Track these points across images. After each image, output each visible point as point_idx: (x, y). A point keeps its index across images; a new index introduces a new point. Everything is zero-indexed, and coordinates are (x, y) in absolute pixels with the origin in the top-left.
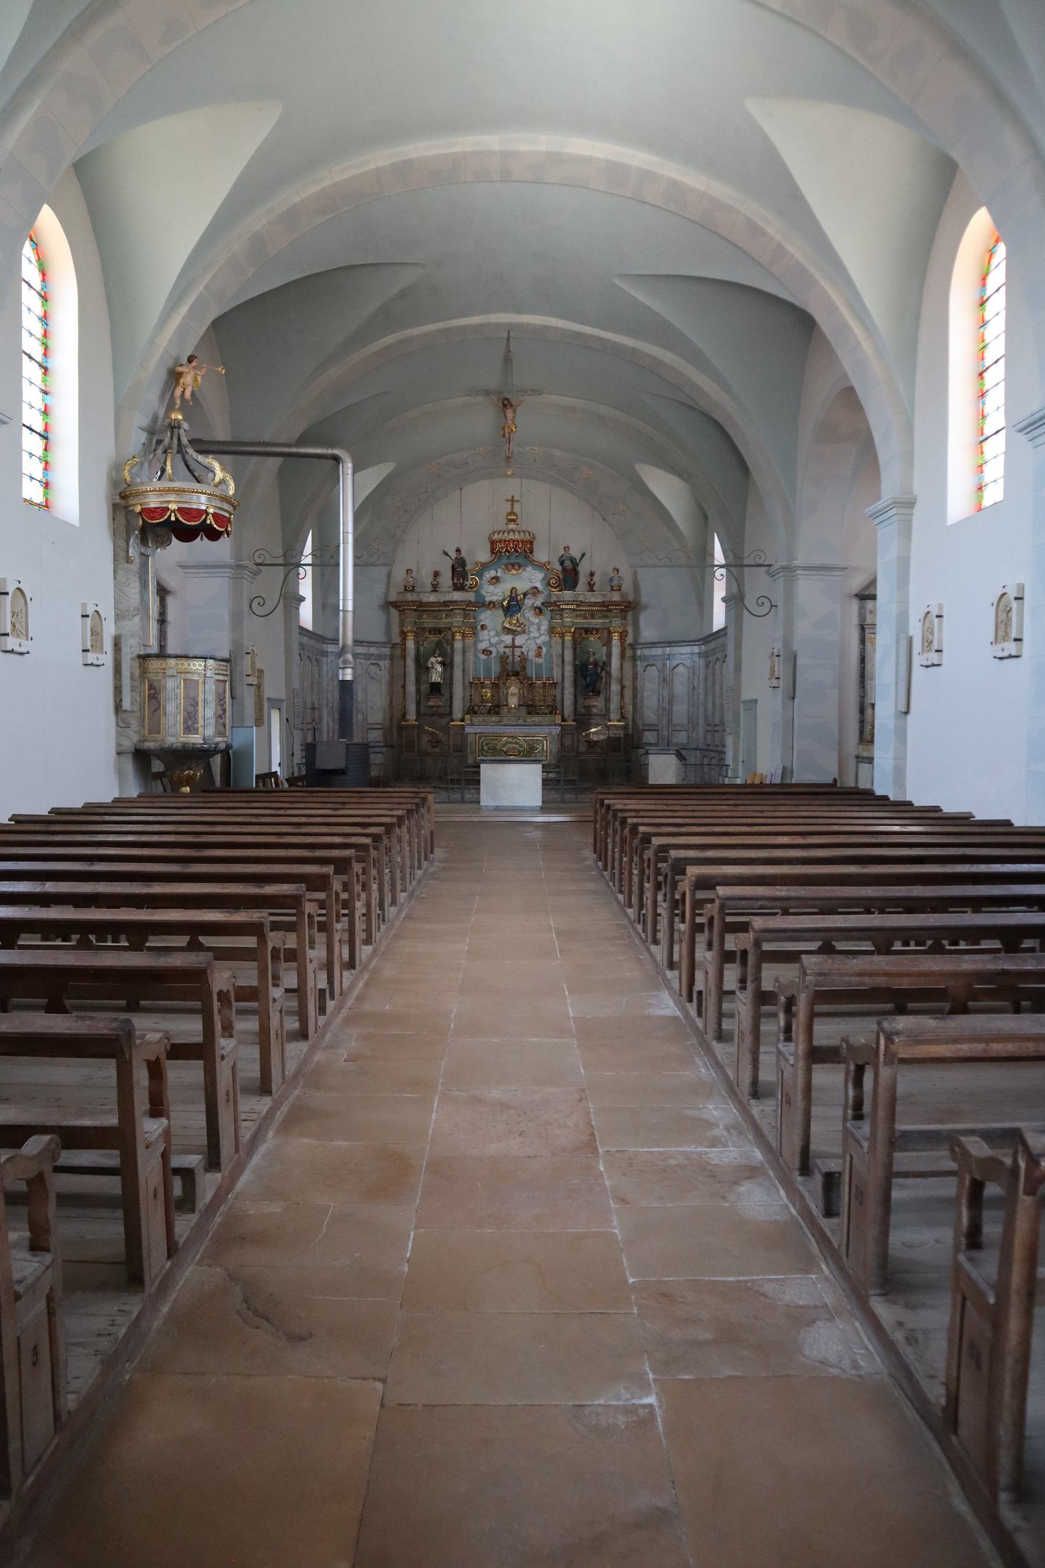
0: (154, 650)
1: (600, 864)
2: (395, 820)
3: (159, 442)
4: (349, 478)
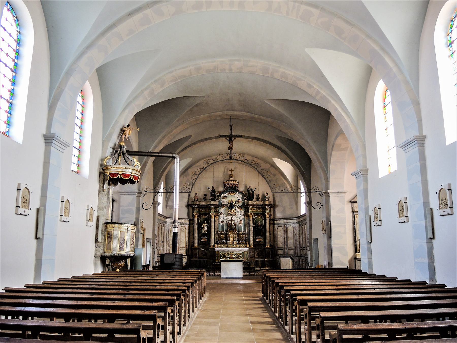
0: (110, 221)
1: (265, 298)
2: (194, 281)
3: (116, 151)
4: (178, 164)
